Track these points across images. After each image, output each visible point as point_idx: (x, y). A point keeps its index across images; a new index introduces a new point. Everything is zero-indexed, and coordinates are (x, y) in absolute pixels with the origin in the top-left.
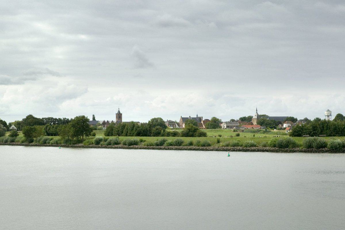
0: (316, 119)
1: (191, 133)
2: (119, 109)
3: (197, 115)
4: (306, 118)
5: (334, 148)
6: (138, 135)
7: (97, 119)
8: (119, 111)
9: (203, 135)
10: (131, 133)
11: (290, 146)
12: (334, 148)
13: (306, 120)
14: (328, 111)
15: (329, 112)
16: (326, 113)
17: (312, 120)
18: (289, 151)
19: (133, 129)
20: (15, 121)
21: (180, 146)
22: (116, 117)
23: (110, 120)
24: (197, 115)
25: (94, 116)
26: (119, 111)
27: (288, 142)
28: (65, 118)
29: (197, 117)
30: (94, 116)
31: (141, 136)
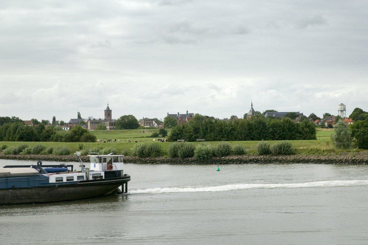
0: (325, 114)
1: (76, 136)
2: (108, 104)
3: (187, 112)
4: (313, 114)
5: (201, 157)
6: (21, 139)
7: (82, 117)
8: (108, 108)
9: (90, 139)
10: (13, 138)
11: (153, 154)
12: (201, 157)
13: (35, 122)
14: (341, 105)
15: (342, 107)
16: (339, 108)
17: (239, 117)
18: (148, 162)
19: (16, 132)
20: (233, 117)
21: (38, 154)
22: (105, 114)
23: (97, 118)
24: (187, 112)
25: (79, 113)
26: (108, 108)
27: (151, 149)
28: (14, 117)
29: (187, 113)
30: (79, 113)
31: (24, 141)
